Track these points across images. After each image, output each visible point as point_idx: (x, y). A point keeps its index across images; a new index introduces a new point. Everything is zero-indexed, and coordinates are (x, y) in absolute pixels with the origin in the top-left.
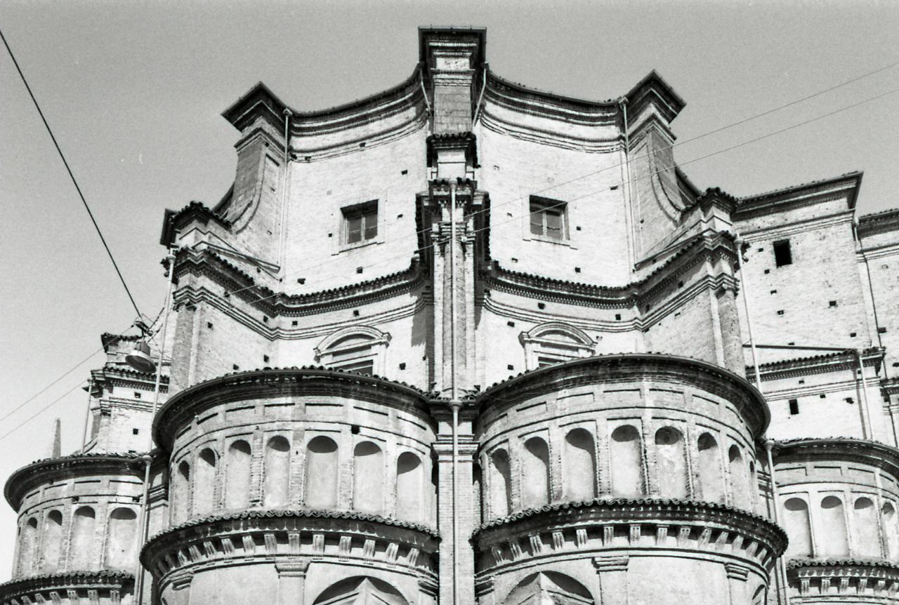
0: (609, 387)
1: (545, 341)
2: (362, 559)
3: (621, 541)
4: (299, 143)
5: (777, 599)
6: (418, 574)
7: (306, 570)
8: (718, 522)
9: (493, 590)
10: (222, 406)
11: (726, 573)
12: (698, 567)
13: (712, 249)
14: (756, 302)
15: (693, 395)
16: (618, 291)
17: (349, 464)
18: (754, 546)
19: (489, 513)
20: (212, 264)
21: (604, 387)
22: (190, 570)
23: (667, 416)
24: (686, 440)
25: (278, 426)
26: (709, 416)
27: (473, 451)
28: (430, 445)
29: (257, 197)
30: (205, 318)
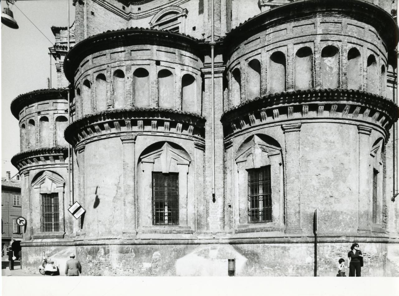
0: (296, 24)
1: (272, 4)
2: (163, 132)
3: (297, 115)
5: (392, 146)
6: (194, 139)
7: (135, 139)
8: (355, 101)
9: (232, 146)
10: (90, 56)
12: (341, 128)
15: (348, 24)
18: (377, 115)
19: (231, 105)
21: (293, 24)
22: (84, 143)
23: (329, 39)
24: (341, 53)
25: (118, 64)
26: (357, 37)
27: (223, 71)
28: (200, 69)
30: (89, 9)
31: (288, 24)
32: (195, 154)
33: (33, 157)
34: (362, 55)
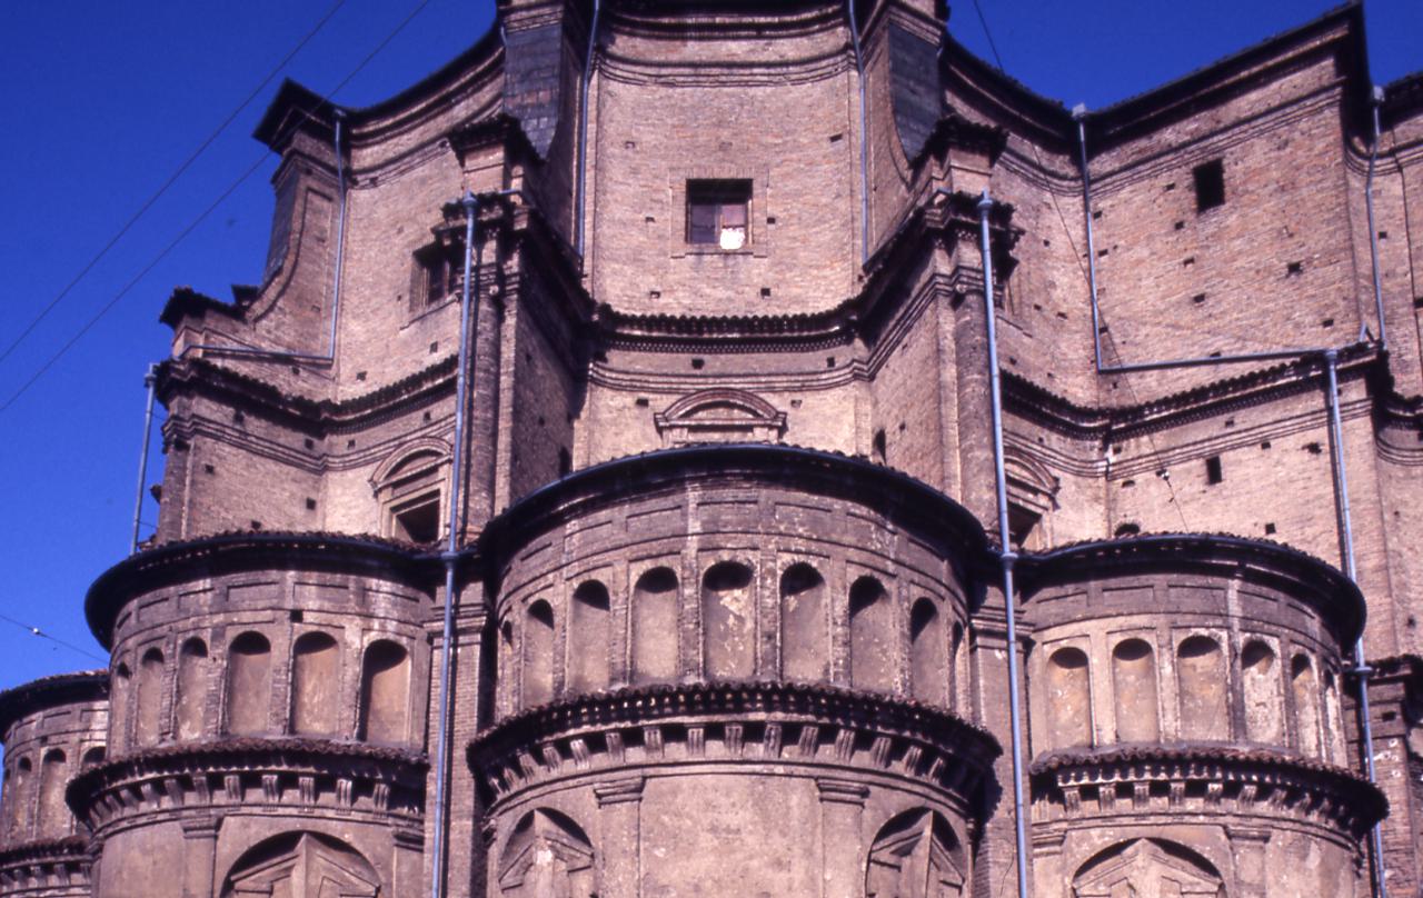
0: (636, 508)
1: (693, 423)
3: (635, 755)
4: (366, 156)
6: (390, 821)
8: (792, 712)
11: (817, 793)
12: (761, 787)
13: (942, 227)
14: (1158, 286)
16: (823, 320)
17: (284, 668)
20: (205, 379)
21: (627, 509)
23: (723, 544)
29: (291, 258)
31: (616, 509)
32: (395, 864)
33: (13, 865)
34: (827, 582)
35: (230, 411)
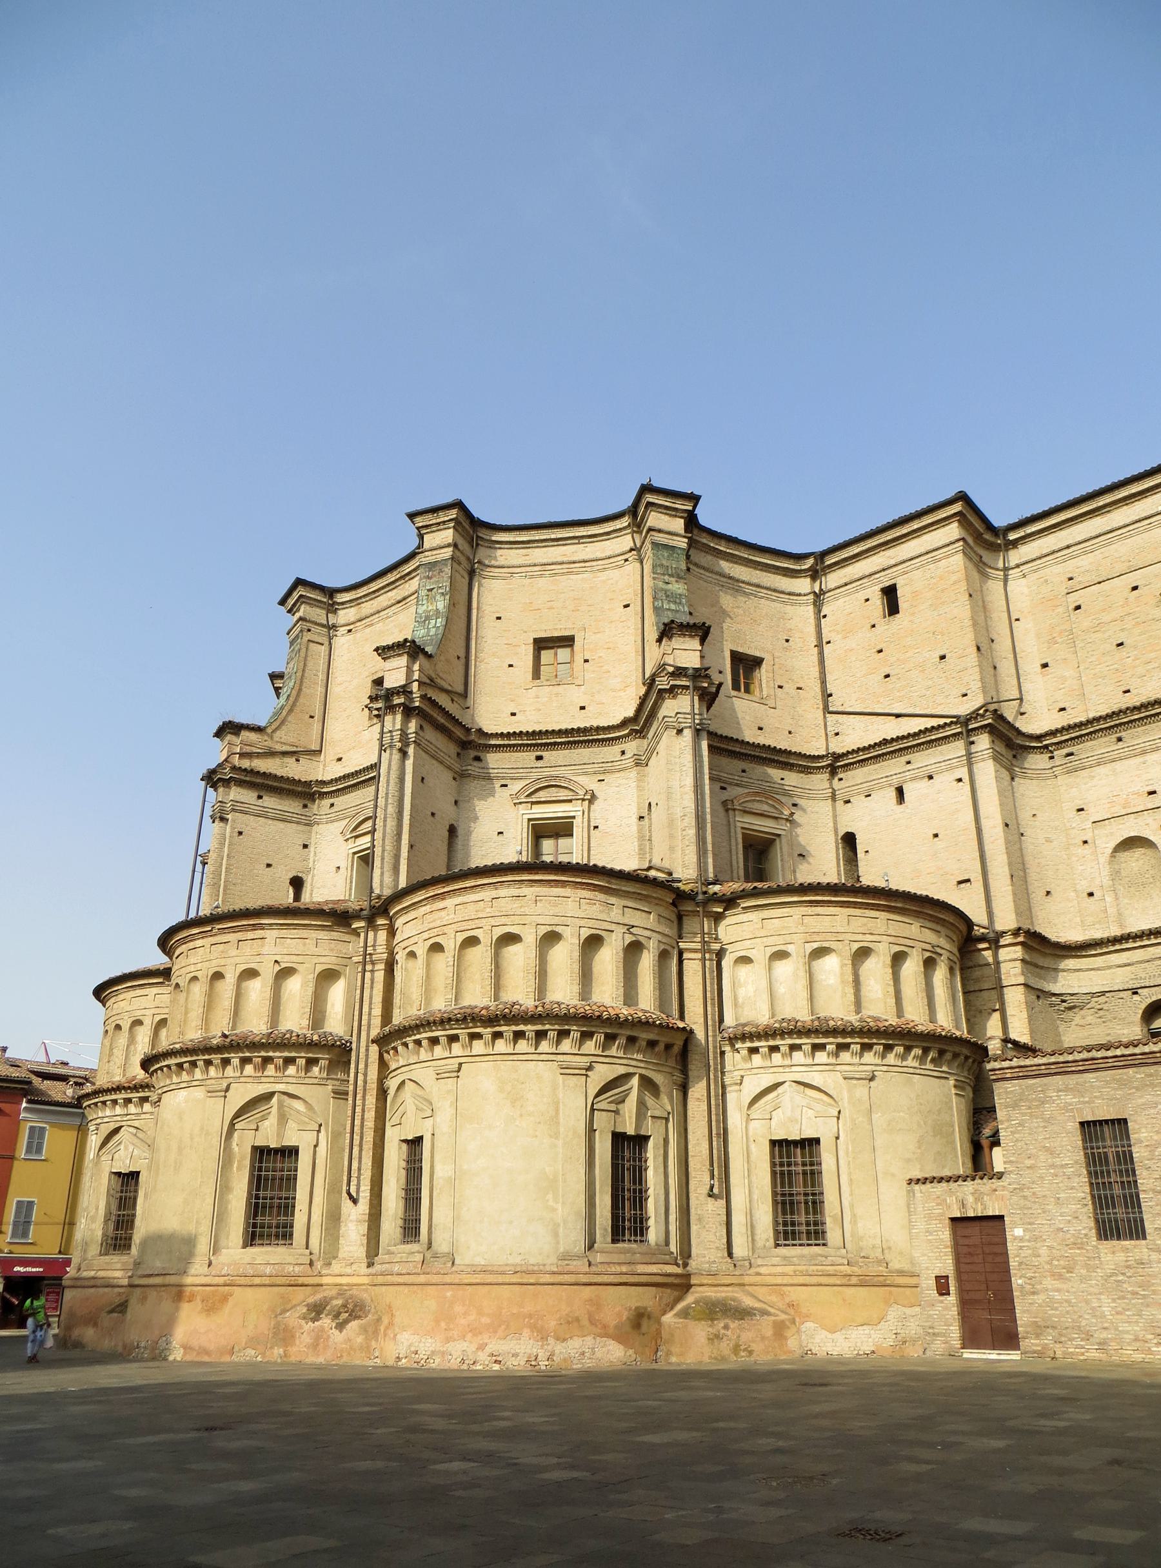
35: (255, 795)
